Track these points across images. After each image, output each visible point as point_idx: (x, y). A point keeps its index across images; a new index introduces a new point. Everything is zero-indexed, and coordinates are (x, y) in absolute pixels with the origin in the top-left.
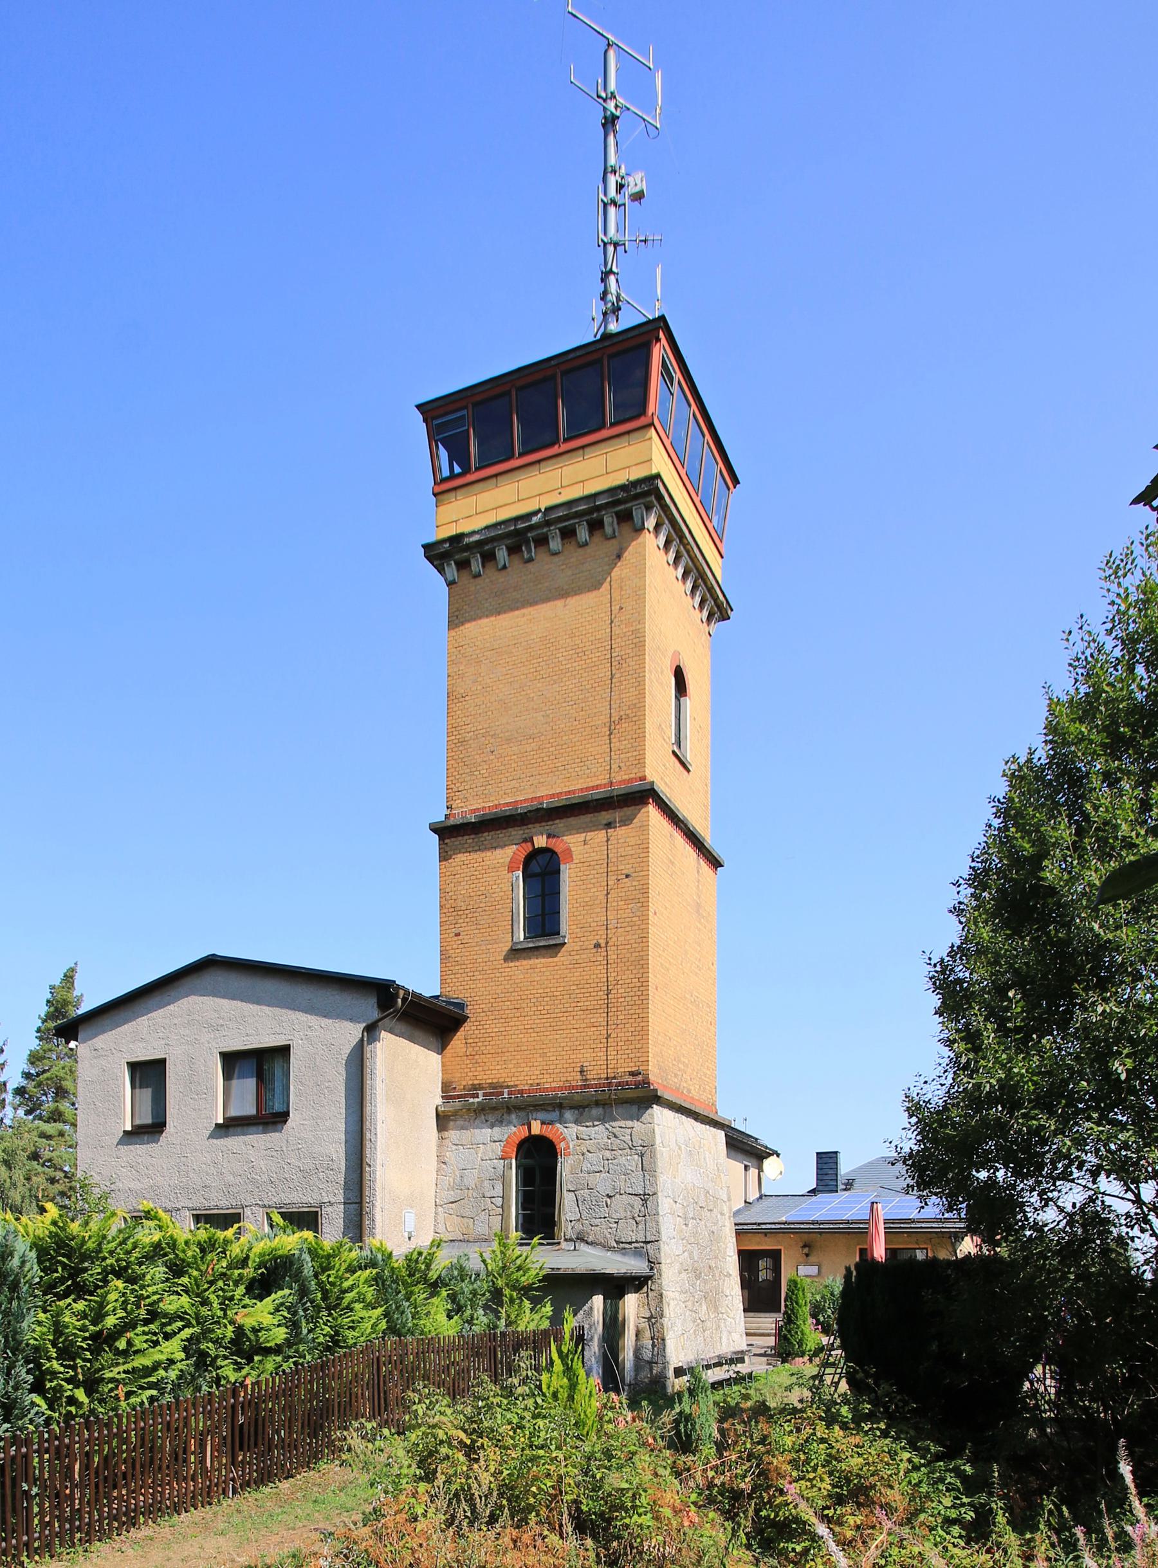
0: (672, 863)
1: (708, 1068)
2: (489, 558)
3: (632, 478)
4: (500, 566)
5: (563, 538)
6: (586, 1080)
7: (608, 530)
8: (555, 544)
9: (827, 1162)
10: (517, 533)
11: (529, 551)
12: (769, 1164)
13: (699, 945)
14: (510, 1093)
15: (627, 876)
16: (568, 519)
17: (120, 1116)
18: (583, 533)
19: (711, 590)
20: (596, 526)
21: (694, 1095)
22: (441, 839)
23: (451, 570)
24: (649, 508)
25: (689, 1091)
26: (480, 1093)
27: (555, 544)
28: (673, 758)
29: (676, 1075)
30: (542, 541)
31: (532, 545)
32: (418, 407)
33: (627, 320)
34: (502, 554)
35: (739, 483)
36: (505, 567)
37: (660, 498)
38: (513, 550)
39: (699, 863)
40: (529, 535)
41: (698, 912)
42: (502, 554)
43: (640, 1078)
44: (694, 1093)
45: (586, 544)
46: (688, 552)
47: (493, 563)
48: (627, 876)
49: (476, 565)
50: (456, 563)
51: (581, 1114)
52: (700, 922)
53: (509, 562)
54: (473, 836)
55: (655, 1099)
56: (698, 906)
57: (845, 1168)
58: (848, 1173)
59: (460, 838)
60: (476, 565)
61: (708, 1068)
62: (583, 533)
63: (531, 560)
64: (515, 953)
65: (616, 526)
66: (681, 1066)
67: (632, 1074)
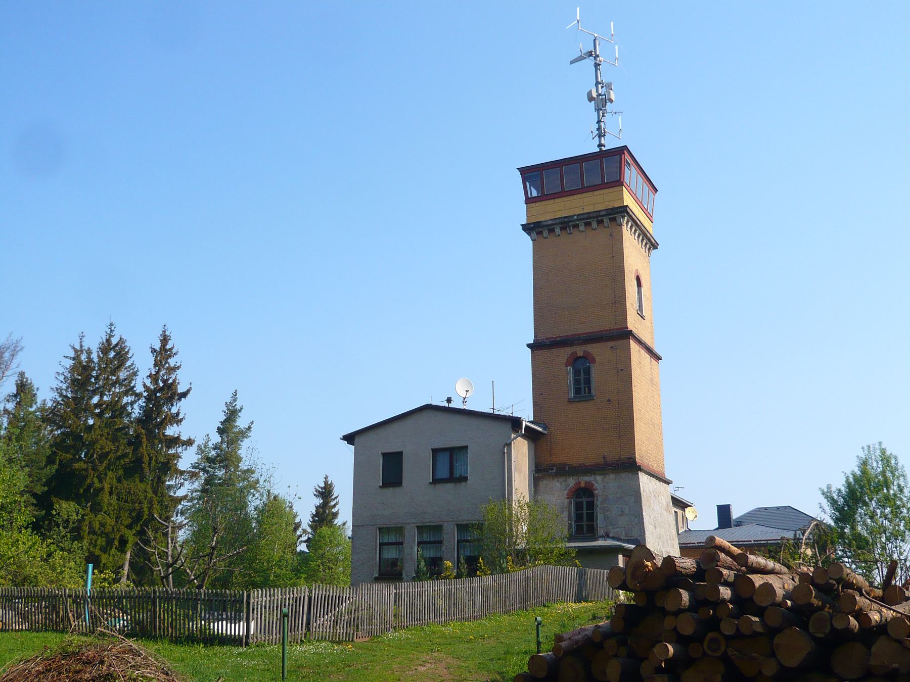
0: (640, 363)
1: (660, 456)
2: (551, 231)
3: (616, 206)
4: (557, 235)
5: (585, 226)
6: (606, 462)
7: (606, 224)
8: (582, 228)
9: (724, 512)
10: (564, 223)
11: (570, 230)
12: (687, 510)
13: (653, 397)
14: (569, 468)
15: (622, 370)
16: (588, 219)
17: (379, 483)
18: (594, 225)
19: (649, 240)
20: (600, 222)
21: (654, 466)
22: (532, 351)
23: (534, 234)
24: (623, 217)
25: (652, 466)
26: (555, 468)
27: (582, 228)
28: (657, 350)
29: (647, 459)
30: (576, 226)
31: (572, 228)
32: (518, 169)
33: (610, 143)
34: (558, 230)
35: (657, 191)
36: (559, 235)
37: (628, 213)
38: (562, 229)
39: (651, 360)
40: (570, 224)
41: (652, 383)
42: (558, 230)
43: (632, 460)
44: (655, 468)
45: (596, 229)
46: (639, 228)
47: (554, 233)
48: (622, 370)
49: (545, 233)
50: (536, 232)
51: (605, 477)
52: (653, 387)
53: (561, 233)
54: (547, 350)
55: (639, 469)
56: (652, 379)
57: (735, 514)
58: (738, 518)
59: (541, 351)
60: (545, 233)
61: (660, 456)
62: (594, 225)
63: (571, 233)
64: (570, 401)
65: (609, 223)
66: (648, 455)
67: (628, 458)
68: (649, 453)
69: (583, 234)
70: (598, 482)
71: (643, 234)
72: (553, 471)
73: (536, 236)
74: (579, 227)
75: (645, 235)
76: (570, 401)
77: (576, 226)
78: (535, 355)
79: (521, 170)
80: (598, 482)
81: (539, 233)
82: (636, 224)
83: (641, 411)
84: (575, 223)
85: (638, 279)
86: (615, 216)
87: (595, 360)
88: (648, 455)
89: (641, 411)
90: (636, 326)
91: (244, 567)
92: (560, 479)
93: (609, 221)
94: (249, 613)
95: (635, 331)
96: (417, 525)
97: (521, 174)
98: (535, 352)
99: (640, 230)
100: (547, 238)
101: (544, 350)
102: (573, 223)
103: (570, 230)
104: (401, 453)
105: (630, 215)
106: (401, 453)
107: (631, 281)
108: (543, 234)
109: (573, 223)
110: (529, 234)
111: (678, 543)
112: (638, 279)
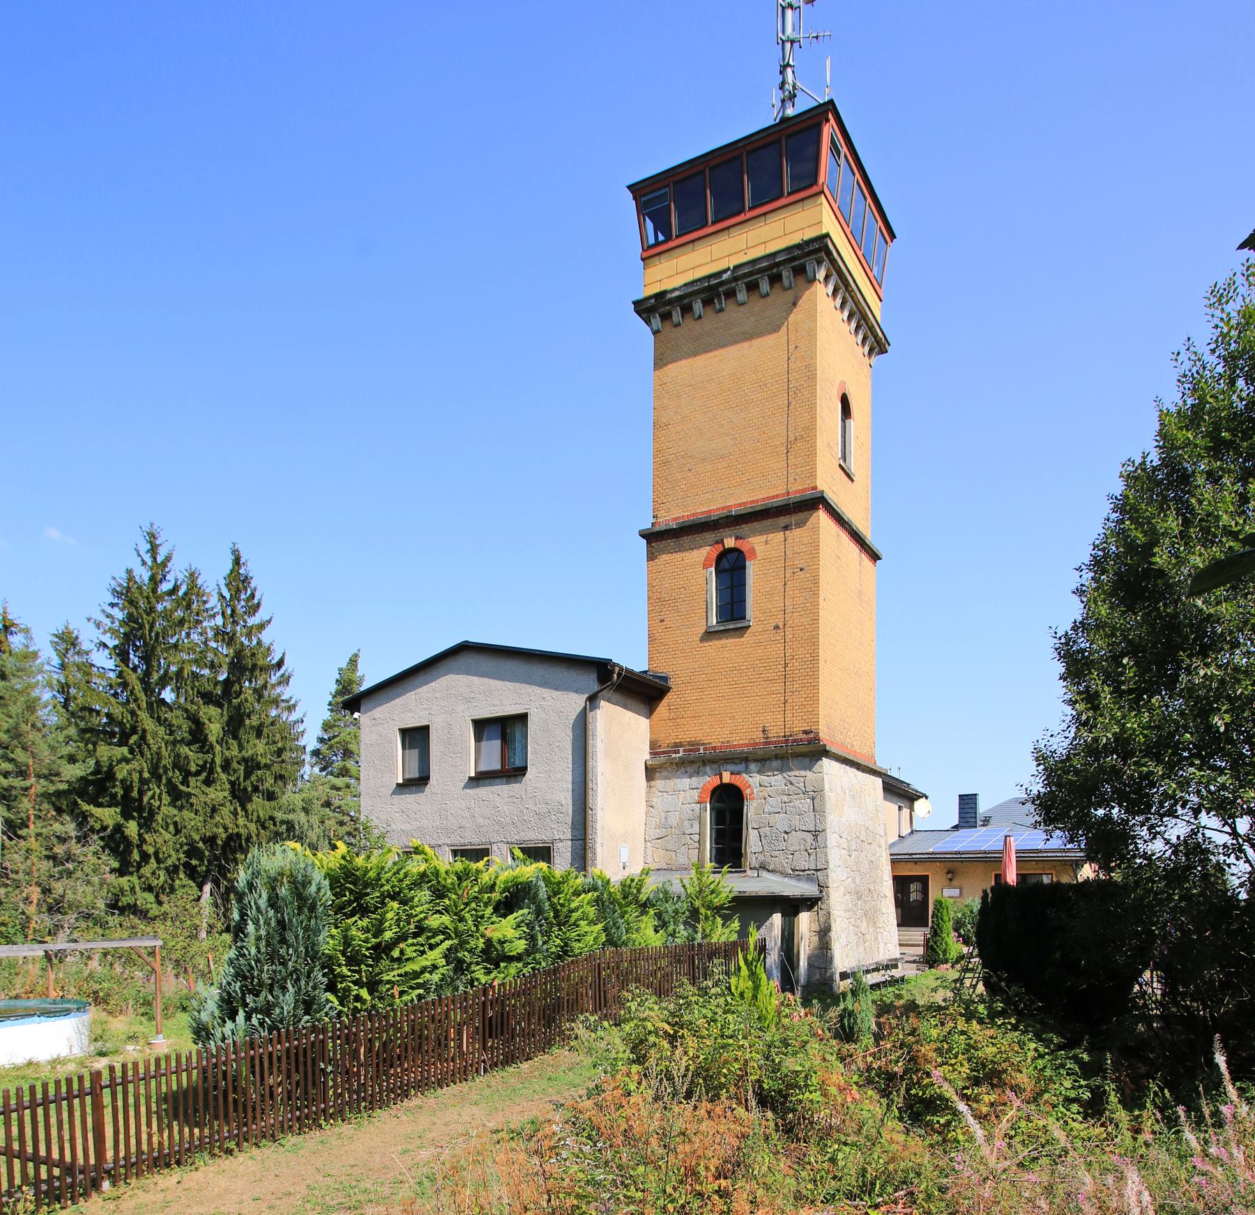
0: (839, 558)
1: (868, 727)
2: (687, 310)
6: (767, 738)
7: (786, 282)
9: (967, 803)
10: (710, 288)
11: (720, 303)
15: (801, 570)
18: (764, 286)
19: (871, 329)
23: (656, 322)
24: (819, 262)
25: (852, 746)
26: (681, 749)
27: (742, 296)
29: (842, 733)
30: (731, 294)
31: (723, 298)
33: (803, 104)
34: (698, 306)
36: (700, 317)
37: (829, 253)
38: (707, 303)
39: (861, 558)
41: (860, 597)
42: (698, 306)
43: (812, 735)
44: (857, 748)
45: (767, 295)
46: (852, 297)
48: (801, 570)
49: (677, 316)
55: (825, 753)
56: (860, 592)
60: (677, 316)
61: (868, 727)
62: (764, 286)
63: (721, 310)
64: (709, 635)
67: (806, 732)
70: (753, 782)
75: (864, 317)
81: (666, 317)
84: (728, 286)
85: (845, 401)
86: (802, 261)
90: (835, 489)
91: (100, 983)
92: (689, 769)
94: (46, 1140)
95: (829, 495)
97: (635, 198)
99: (854, 301)
102: (724, 288)
104: (426, 728)
106: (426, 728)
107: (830, 399)
109: (724, 288)
111: (897, 942)
112: (845, 401)
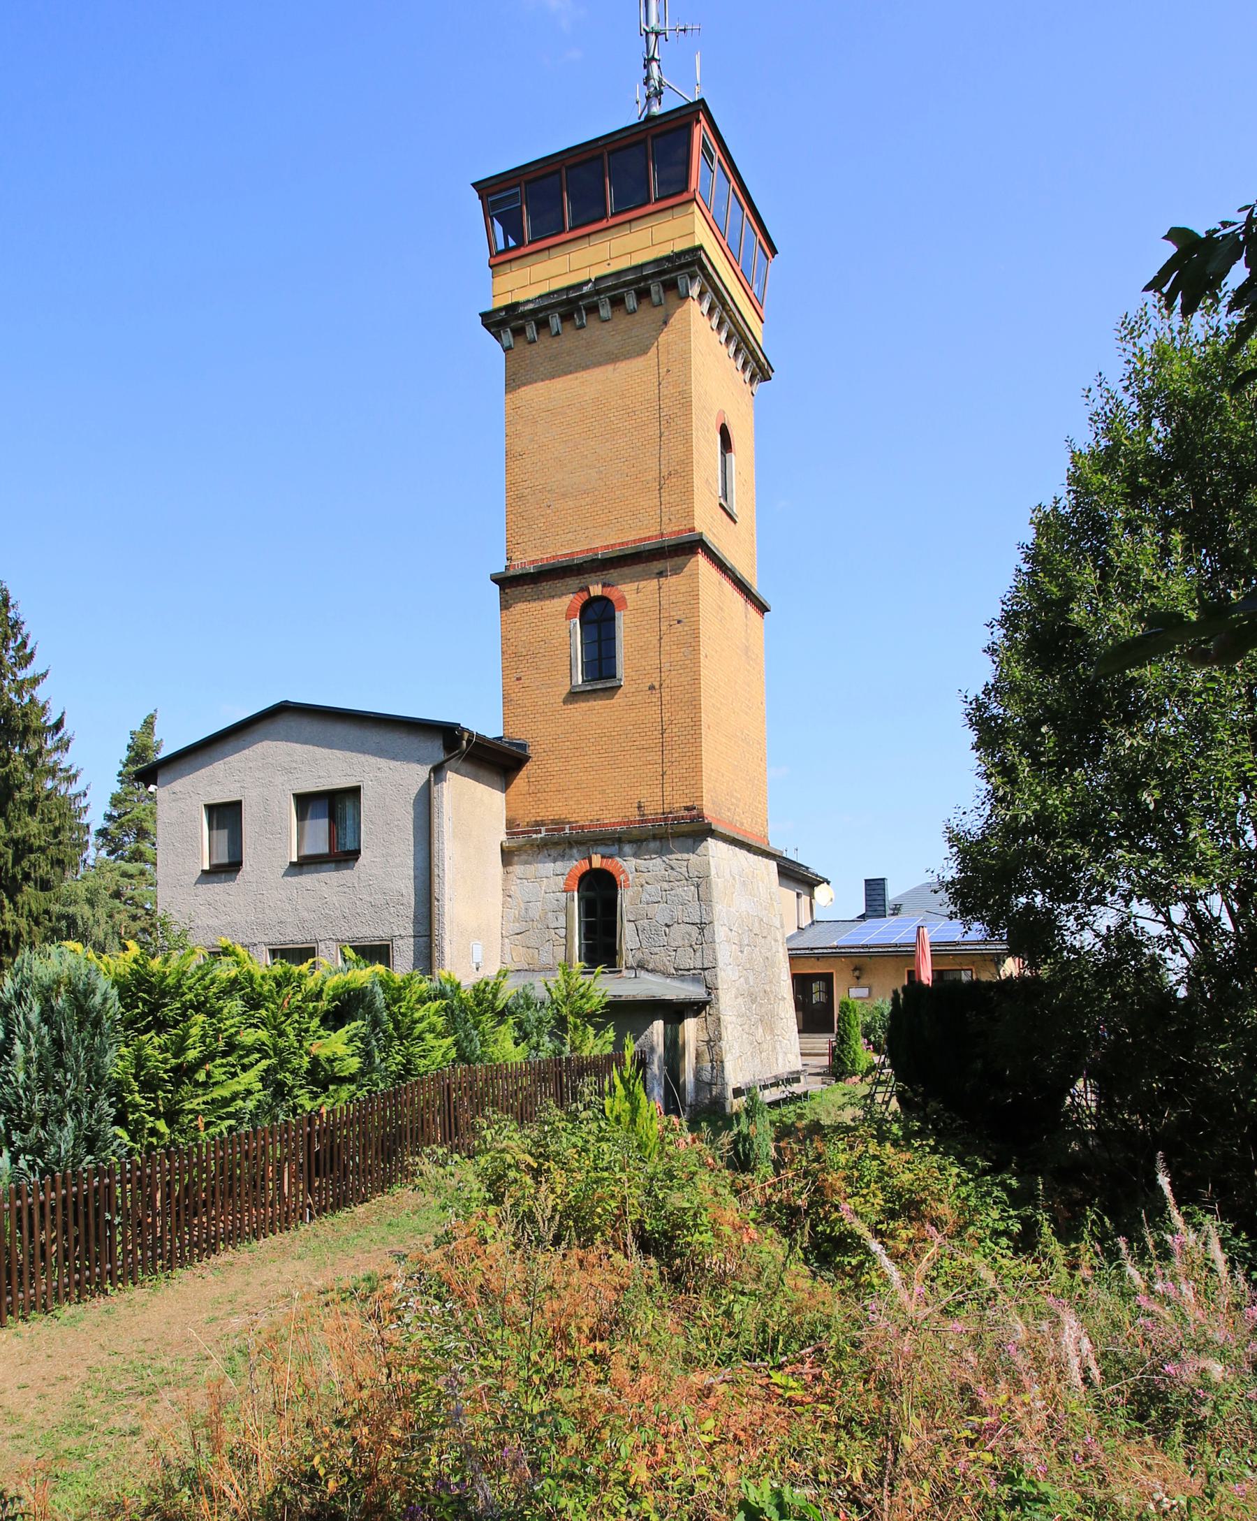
0: (722, 609)
2: (543, 325)
5: (612, 306)
6: (644, 815)
7: (655, 298)
8: (605, 312)
9: (875, 888)
10: (569, 301)
11: (581, 319)
15: (679, 622)
17: (197, 855)
18: (631, 302)
21: (745, 826)
23: (508, 337)
24: (693, 277)
25: (742, 824)
27: (605, 312)
29: (729, 809)
31: (584, 312)
34: (555, 321)
36: (558, 334)
37: (703, 268)
38: (566, 318)
39: (747, 609)
41: (746, 654)
42: (555, 321)
44: (746, 827)
46: (730, 317)
48: (679, 622)
49: (531, 331)
50: (512, 330)
52: (749, 664)
53: (563, 329)
58: (895, 899)
59: (520, 588)
63: (582, 327)
66: (733, 800)
67: (688, 809)
68: (736, 798)
69: (606, 325)
70: (628, 867)
71: (739, 333)
72: (539, 836)
73: (511, 339)
74: (598, 311)
76: (574, 696)
77: (593, 309)
78: (508, 598)
79: (480, 186)
80: (628, 867)
81: (519, 332)
82: (720, 305)
83: (719, 709)
87: (626, 603)
88: (733, 800)
89: (719, 709)
93: (662, 291)
96: (271, 947)
97: (480, 197)
98: (507, 591)
100: (535, 341)
101: (526, 587)
103: (581, 319)
104: (238, 804)
105: (709, 274)
106: (238, 804)
107: (708, 431)
108: (525, 333)
110: (498, 337)
111: (798, 1051)
112: (724, 432)
